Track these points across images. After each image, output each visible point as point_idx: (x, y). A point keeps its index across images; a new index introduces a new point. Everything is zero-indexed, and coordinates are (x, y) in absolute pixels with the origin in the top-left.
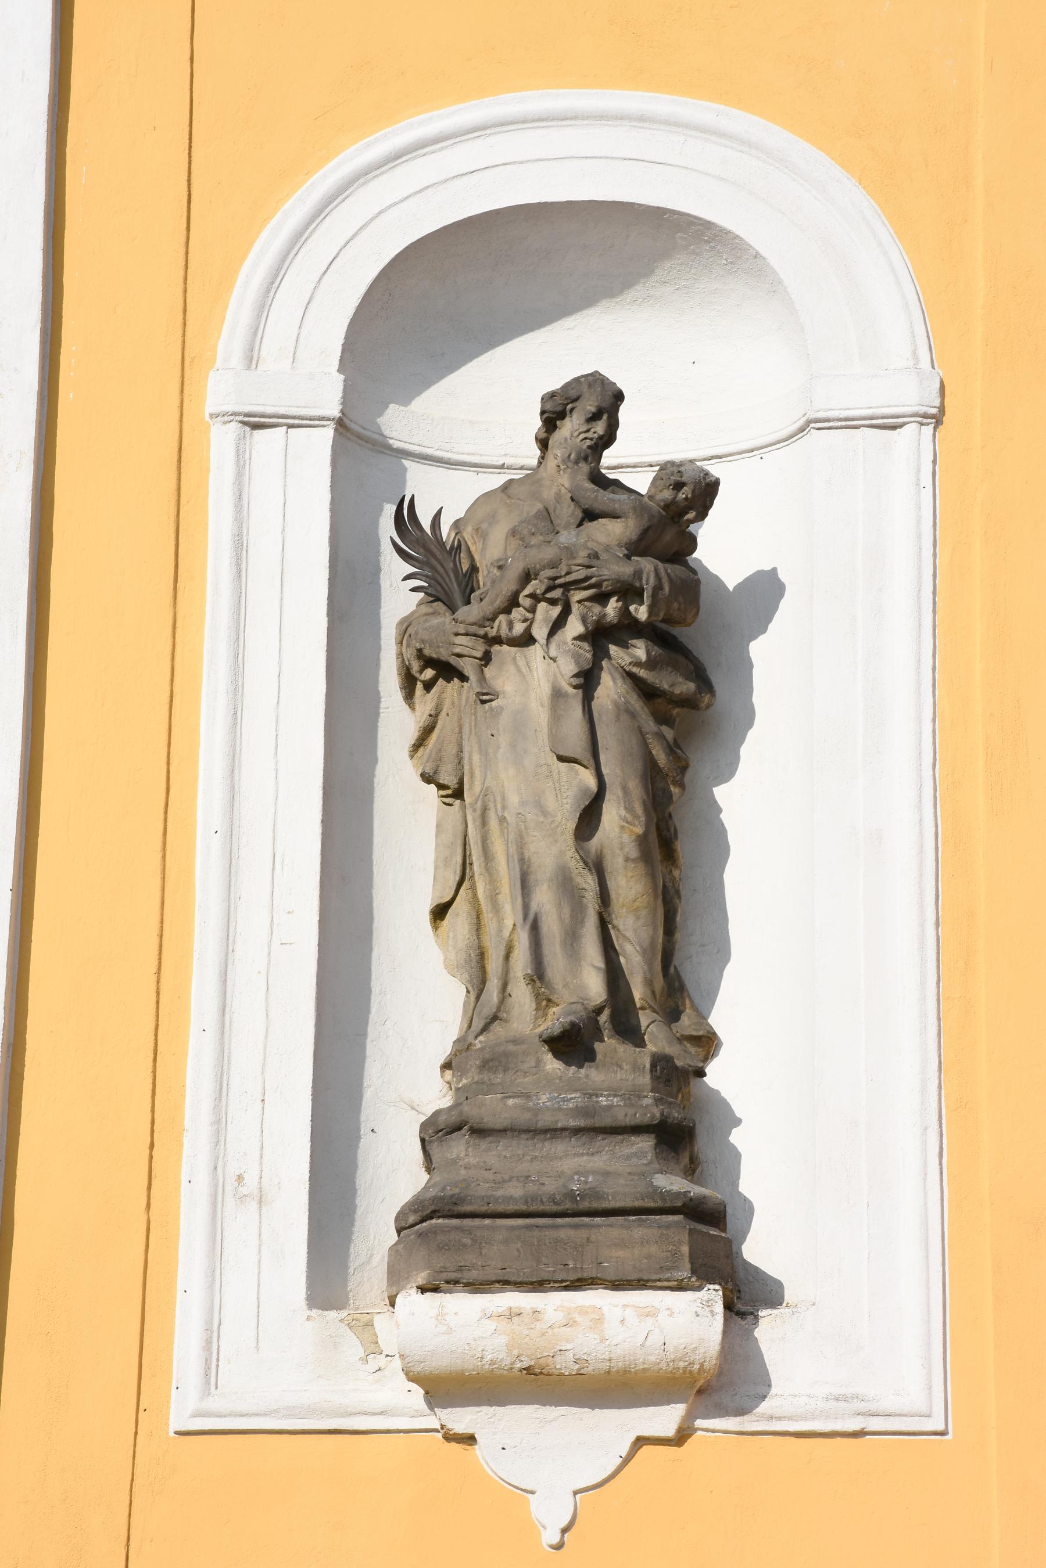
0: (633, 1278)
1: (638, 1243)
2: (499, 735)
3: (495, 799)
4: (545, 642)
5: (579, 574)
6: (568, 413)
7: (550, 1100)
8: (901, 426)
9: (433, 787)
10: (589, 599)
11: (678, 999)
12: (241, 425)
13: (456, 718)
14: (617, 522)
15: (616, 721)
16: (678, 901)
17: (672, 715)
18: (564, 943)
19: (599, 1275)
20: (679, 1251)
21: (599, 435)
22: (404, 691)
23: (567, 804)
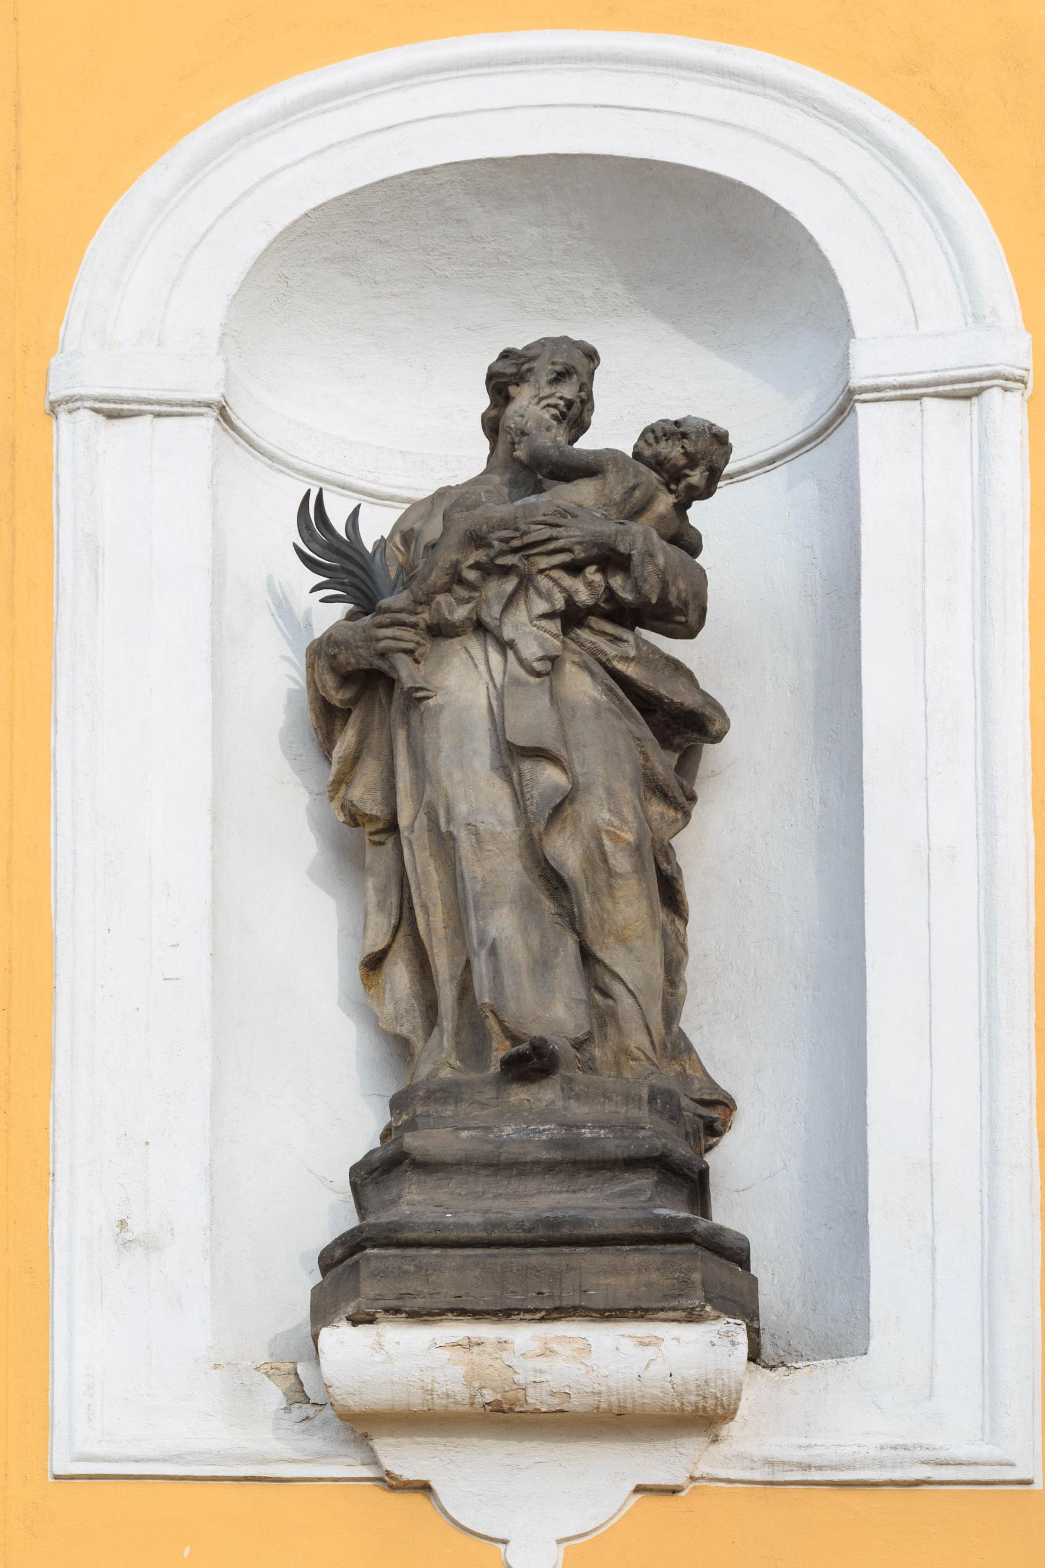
0: (628, 1307)
1: (634, 1270)
7: (517, 1131)
11: (685, 1062)
12: (92, 413)
19: (583, 1304)
23: (532, 805)
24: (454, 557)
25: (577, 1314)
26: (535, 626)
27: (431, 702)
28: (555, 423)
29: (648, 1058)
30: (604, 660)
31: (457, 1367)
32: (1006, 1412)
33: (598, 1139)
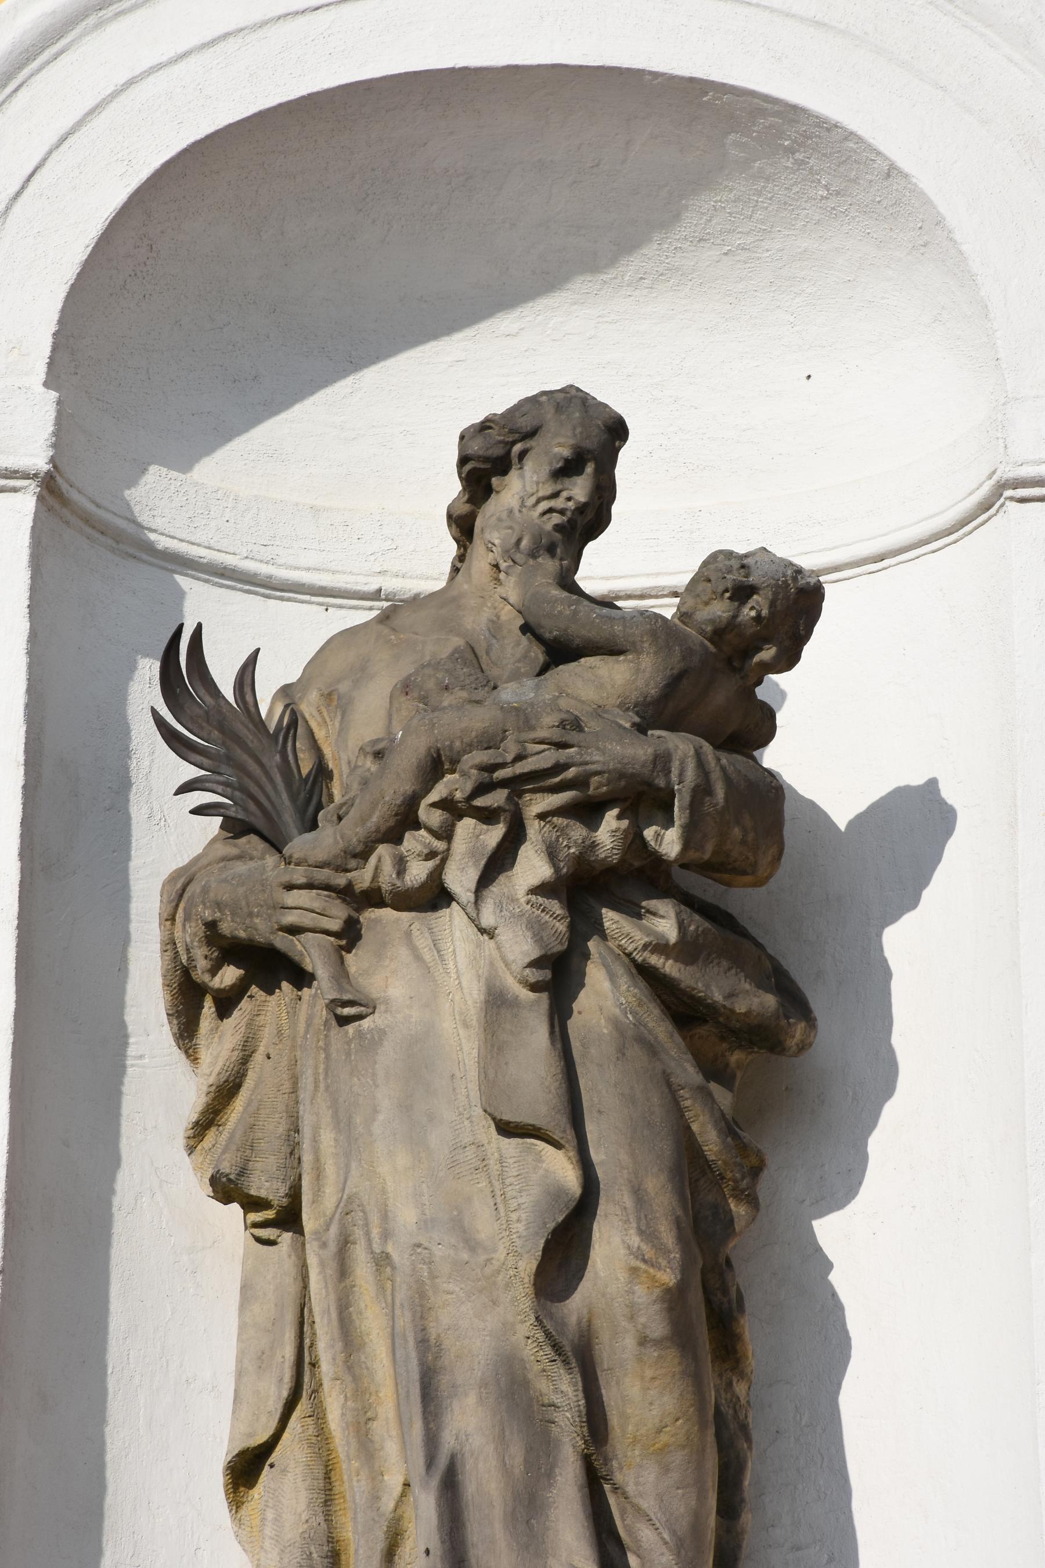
2: (377, 1086)
3: (366, 1219)
4: (471, 897)
5: (542, 759)
6: (515, 460)
9: (235, 1208)
10: (559, 812)
13: (285, 1062)
14: (618, 662)
15: (618, 1059)
16: (745, 1446)
17: (727, 1065)
18: (512, 1519)
21: (577, 502)
22: (175, 1022)
23: (518, 1221)
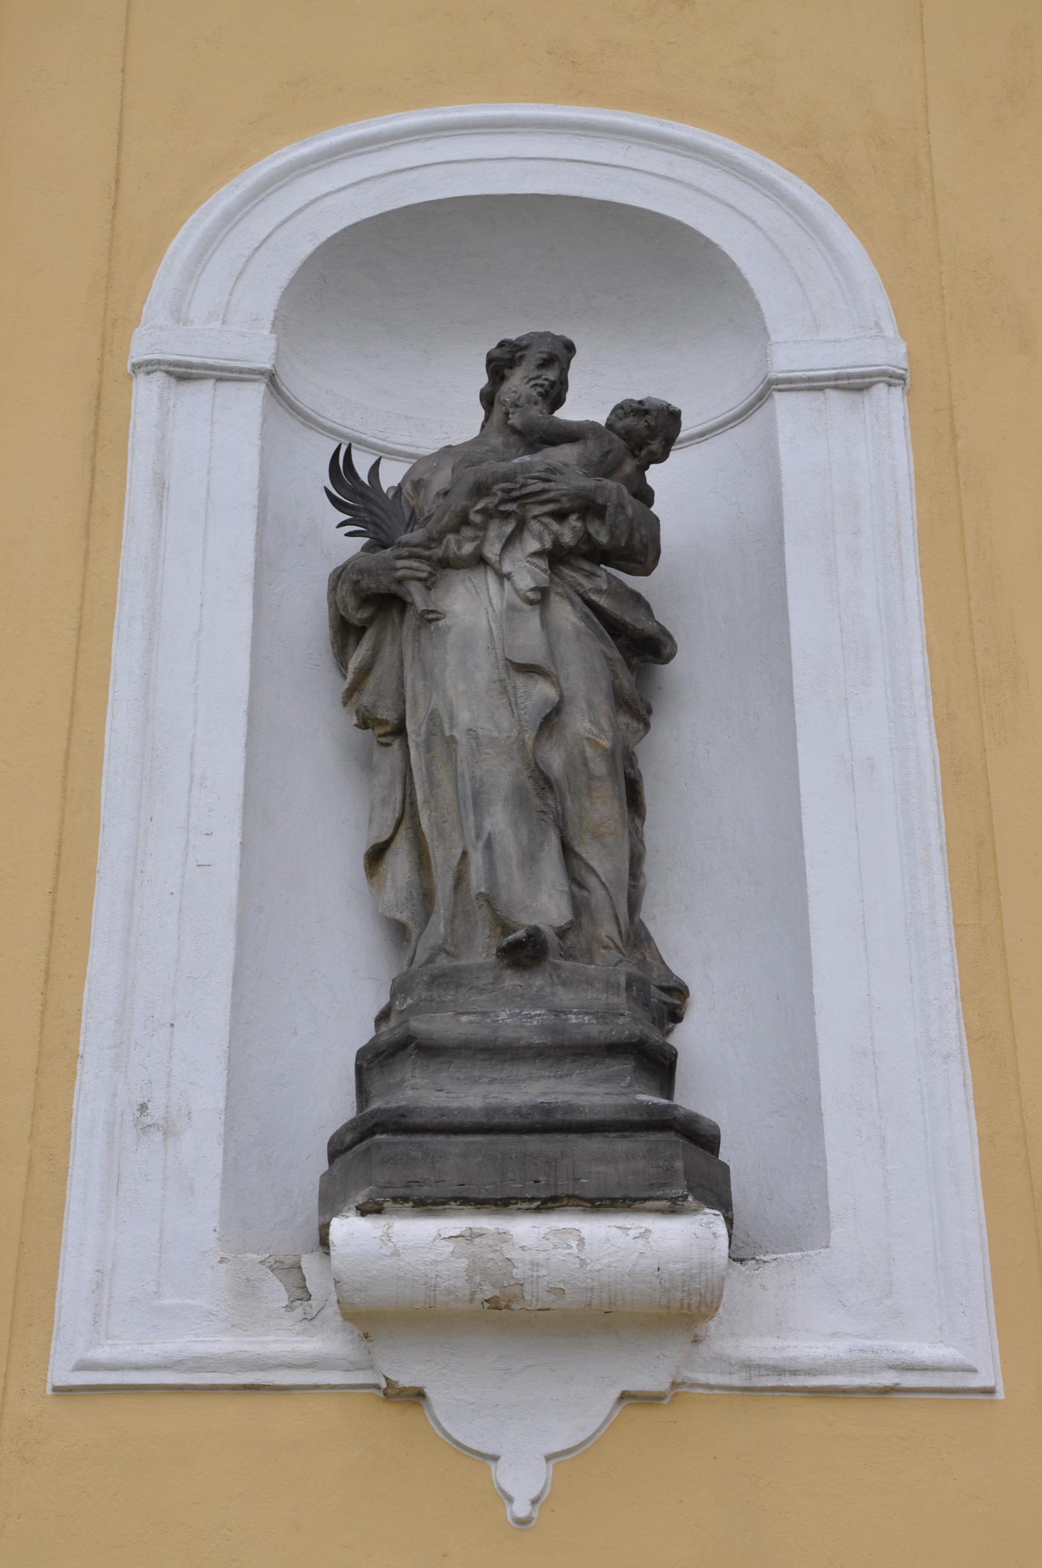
0: (617, 1196)
7: (511, 1016)
8: (867, 387)
10: (545, 514)
11: (646, 950)
12: (165, 375)
19: (576, 1192)
20: (672, 1167)
22: (335, 647)
23: (525, 714)
24: (464, 503)
25: (570, 1204)
26: (528, 562)
27: (441, 623)
28: (540, 398)
29: (617, 946)
30: (582, 591)
31: (459, 1260)
32: (963, 1312)
33: (583, 1024)
